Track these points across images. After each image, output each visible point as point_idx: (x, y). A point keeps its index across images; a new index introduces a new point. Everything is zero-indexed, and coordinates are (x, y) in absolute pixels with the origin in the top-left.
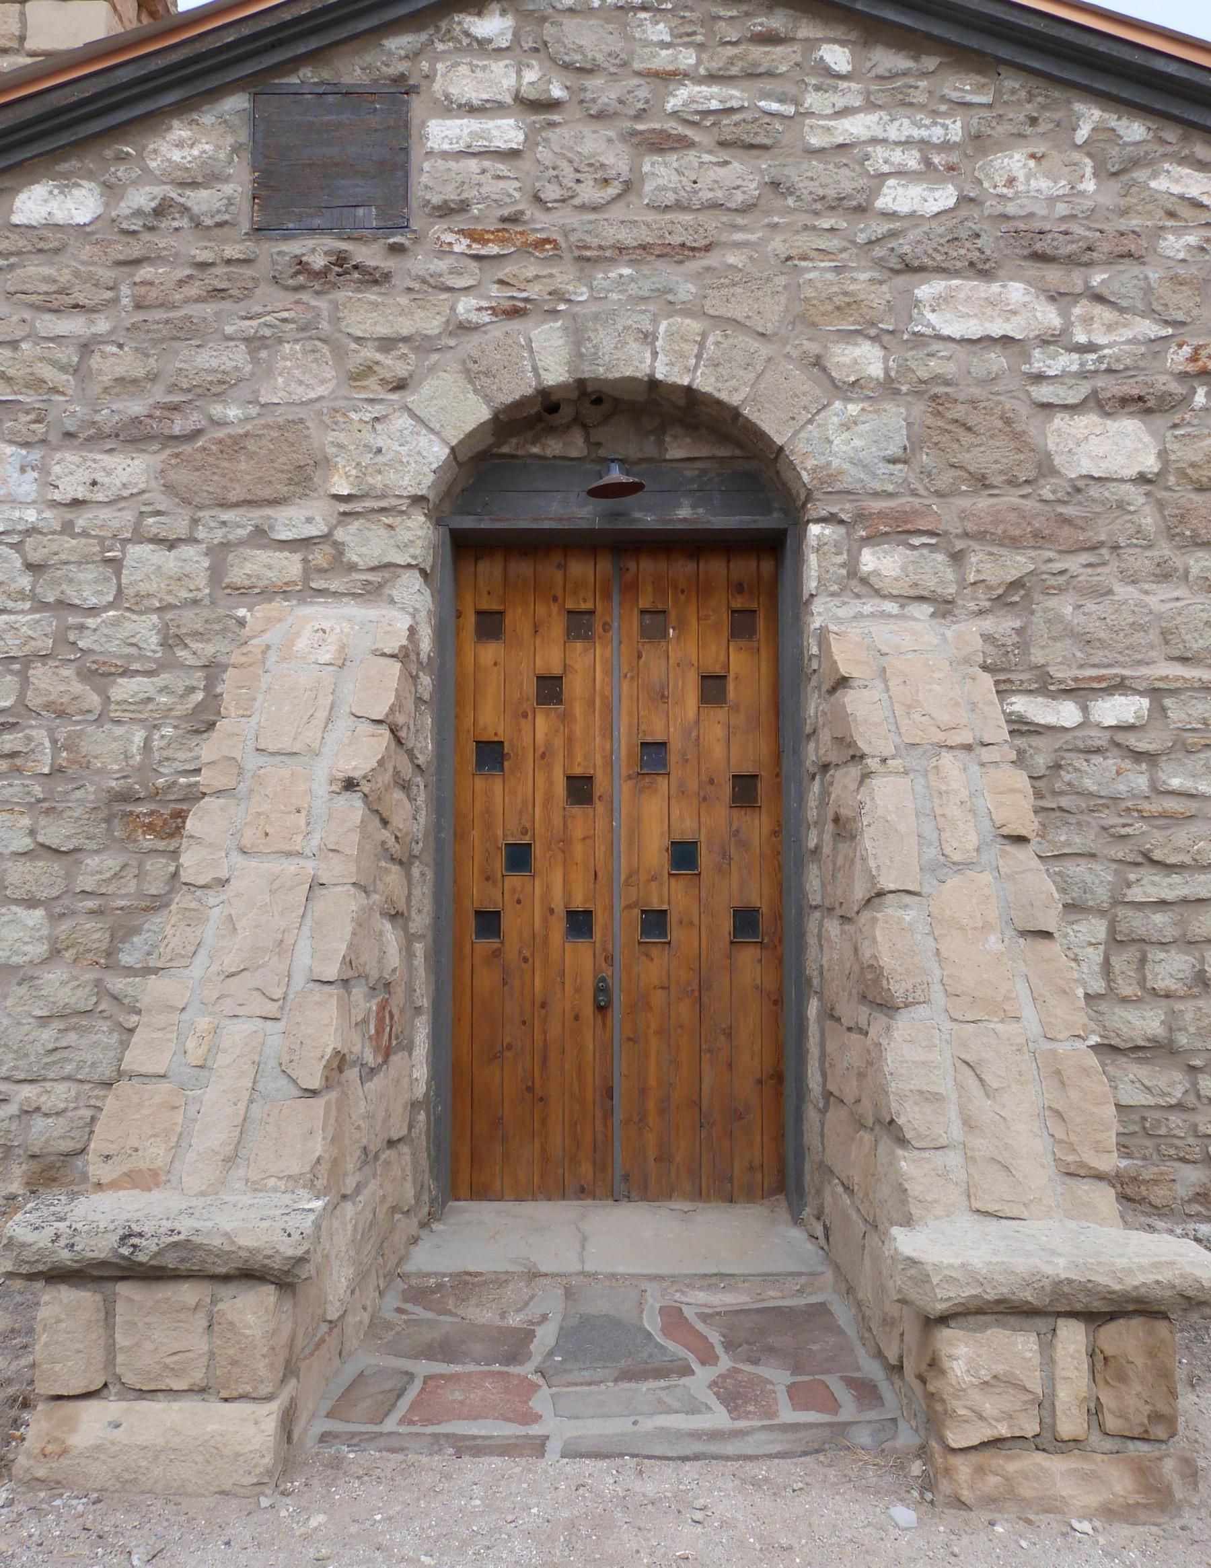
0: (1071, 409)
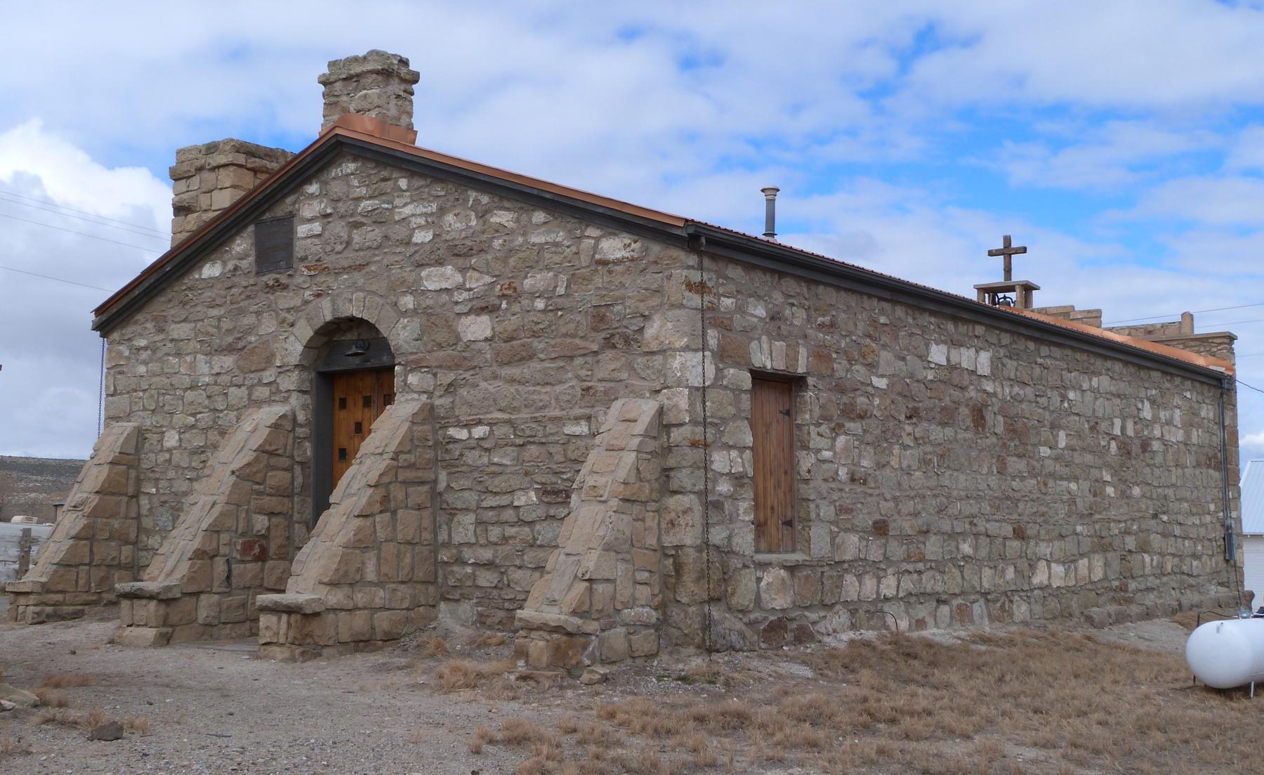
0: (467, 314)
